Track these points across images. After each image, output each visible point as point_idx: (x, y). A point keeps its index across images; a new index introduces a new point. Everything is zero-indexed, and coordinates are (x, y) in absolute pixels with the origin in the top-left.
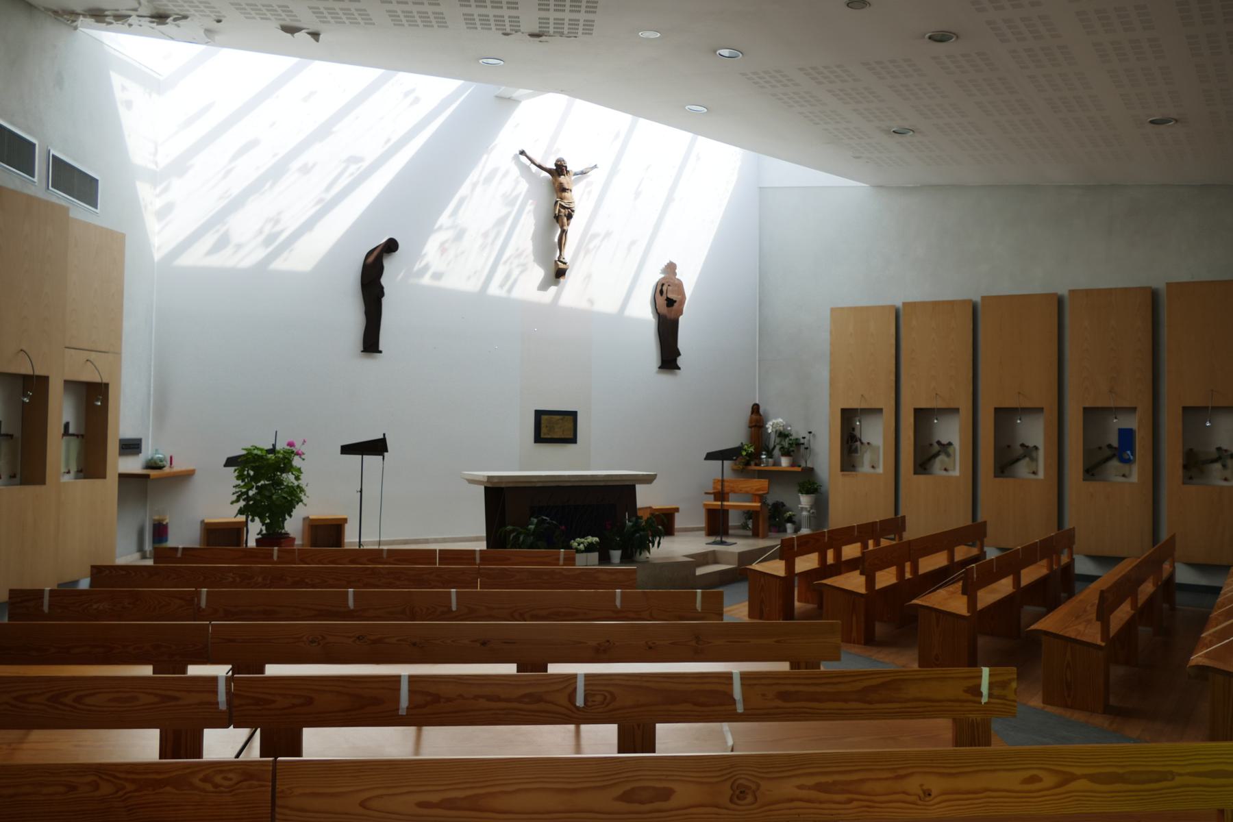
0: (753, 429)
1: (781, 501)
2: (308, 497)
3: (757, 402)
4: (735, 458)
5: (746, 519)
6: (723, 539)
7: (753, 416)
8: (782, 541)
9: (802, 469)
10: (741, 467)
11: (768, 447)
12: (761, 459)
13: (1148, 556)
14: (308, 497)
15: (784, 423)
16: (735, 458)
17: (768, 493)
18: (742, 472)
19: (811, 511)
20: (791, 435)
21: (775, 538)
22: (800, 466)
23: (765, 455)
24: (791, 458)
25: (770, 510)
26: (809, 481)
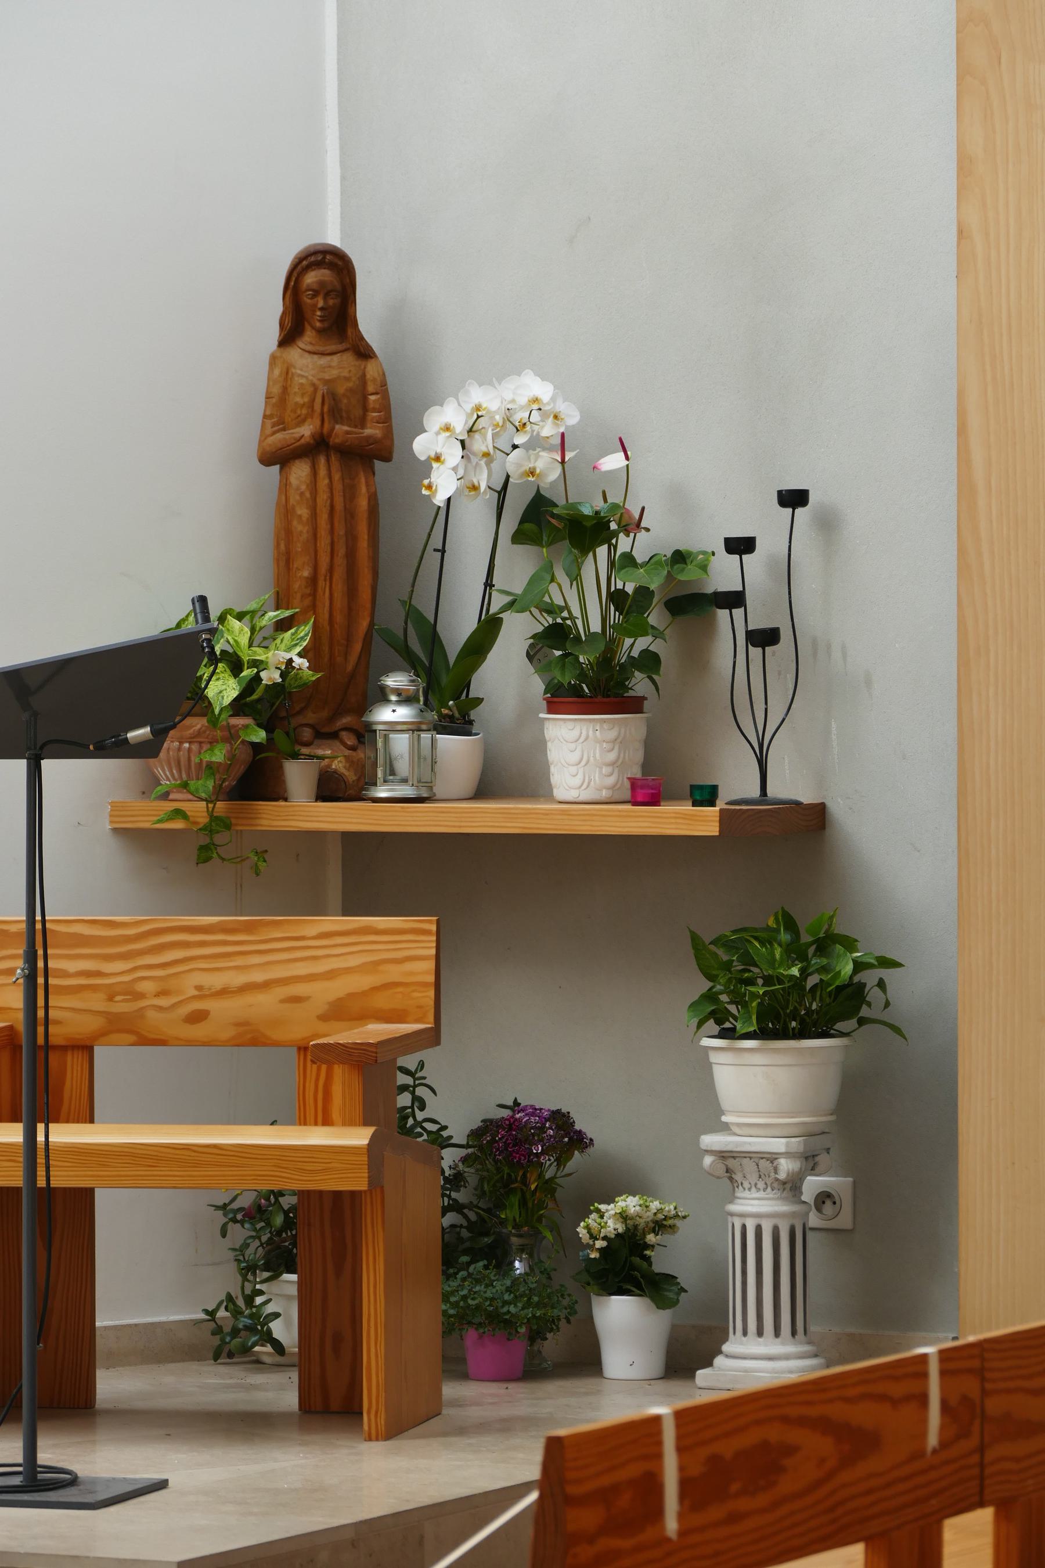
0: (300, 471)
1: (549, 1103)
2: (454, 1161)
3: (333, 238)
4: (138, 734)
5: (248, 1269)
6: (45, 1456)
7: (294, 355)
8: (554, 1447)
9: (725, 817)
10: (198, 810)
11: (433, 640)
12: (365, 734)
13: (356, 1028)
14: (454, 1161)
15: (572, 417)
16: (138, 734)
17: (432, 1037)
18: (205, 853)
19: (813, 1184)
20: (633, 526)
21: (506, 1427)
22: (706, 796)
23: (406, 699)
24: (632, 725)
25: (455, 1180)
26: (790, 924)
